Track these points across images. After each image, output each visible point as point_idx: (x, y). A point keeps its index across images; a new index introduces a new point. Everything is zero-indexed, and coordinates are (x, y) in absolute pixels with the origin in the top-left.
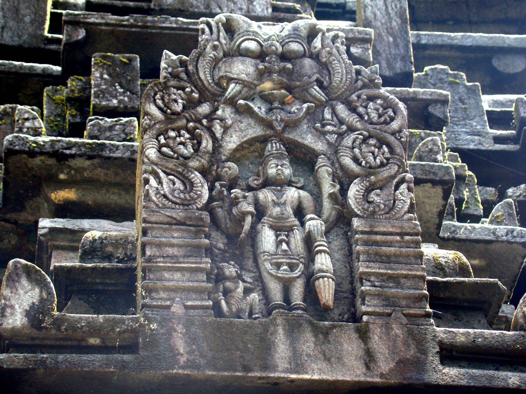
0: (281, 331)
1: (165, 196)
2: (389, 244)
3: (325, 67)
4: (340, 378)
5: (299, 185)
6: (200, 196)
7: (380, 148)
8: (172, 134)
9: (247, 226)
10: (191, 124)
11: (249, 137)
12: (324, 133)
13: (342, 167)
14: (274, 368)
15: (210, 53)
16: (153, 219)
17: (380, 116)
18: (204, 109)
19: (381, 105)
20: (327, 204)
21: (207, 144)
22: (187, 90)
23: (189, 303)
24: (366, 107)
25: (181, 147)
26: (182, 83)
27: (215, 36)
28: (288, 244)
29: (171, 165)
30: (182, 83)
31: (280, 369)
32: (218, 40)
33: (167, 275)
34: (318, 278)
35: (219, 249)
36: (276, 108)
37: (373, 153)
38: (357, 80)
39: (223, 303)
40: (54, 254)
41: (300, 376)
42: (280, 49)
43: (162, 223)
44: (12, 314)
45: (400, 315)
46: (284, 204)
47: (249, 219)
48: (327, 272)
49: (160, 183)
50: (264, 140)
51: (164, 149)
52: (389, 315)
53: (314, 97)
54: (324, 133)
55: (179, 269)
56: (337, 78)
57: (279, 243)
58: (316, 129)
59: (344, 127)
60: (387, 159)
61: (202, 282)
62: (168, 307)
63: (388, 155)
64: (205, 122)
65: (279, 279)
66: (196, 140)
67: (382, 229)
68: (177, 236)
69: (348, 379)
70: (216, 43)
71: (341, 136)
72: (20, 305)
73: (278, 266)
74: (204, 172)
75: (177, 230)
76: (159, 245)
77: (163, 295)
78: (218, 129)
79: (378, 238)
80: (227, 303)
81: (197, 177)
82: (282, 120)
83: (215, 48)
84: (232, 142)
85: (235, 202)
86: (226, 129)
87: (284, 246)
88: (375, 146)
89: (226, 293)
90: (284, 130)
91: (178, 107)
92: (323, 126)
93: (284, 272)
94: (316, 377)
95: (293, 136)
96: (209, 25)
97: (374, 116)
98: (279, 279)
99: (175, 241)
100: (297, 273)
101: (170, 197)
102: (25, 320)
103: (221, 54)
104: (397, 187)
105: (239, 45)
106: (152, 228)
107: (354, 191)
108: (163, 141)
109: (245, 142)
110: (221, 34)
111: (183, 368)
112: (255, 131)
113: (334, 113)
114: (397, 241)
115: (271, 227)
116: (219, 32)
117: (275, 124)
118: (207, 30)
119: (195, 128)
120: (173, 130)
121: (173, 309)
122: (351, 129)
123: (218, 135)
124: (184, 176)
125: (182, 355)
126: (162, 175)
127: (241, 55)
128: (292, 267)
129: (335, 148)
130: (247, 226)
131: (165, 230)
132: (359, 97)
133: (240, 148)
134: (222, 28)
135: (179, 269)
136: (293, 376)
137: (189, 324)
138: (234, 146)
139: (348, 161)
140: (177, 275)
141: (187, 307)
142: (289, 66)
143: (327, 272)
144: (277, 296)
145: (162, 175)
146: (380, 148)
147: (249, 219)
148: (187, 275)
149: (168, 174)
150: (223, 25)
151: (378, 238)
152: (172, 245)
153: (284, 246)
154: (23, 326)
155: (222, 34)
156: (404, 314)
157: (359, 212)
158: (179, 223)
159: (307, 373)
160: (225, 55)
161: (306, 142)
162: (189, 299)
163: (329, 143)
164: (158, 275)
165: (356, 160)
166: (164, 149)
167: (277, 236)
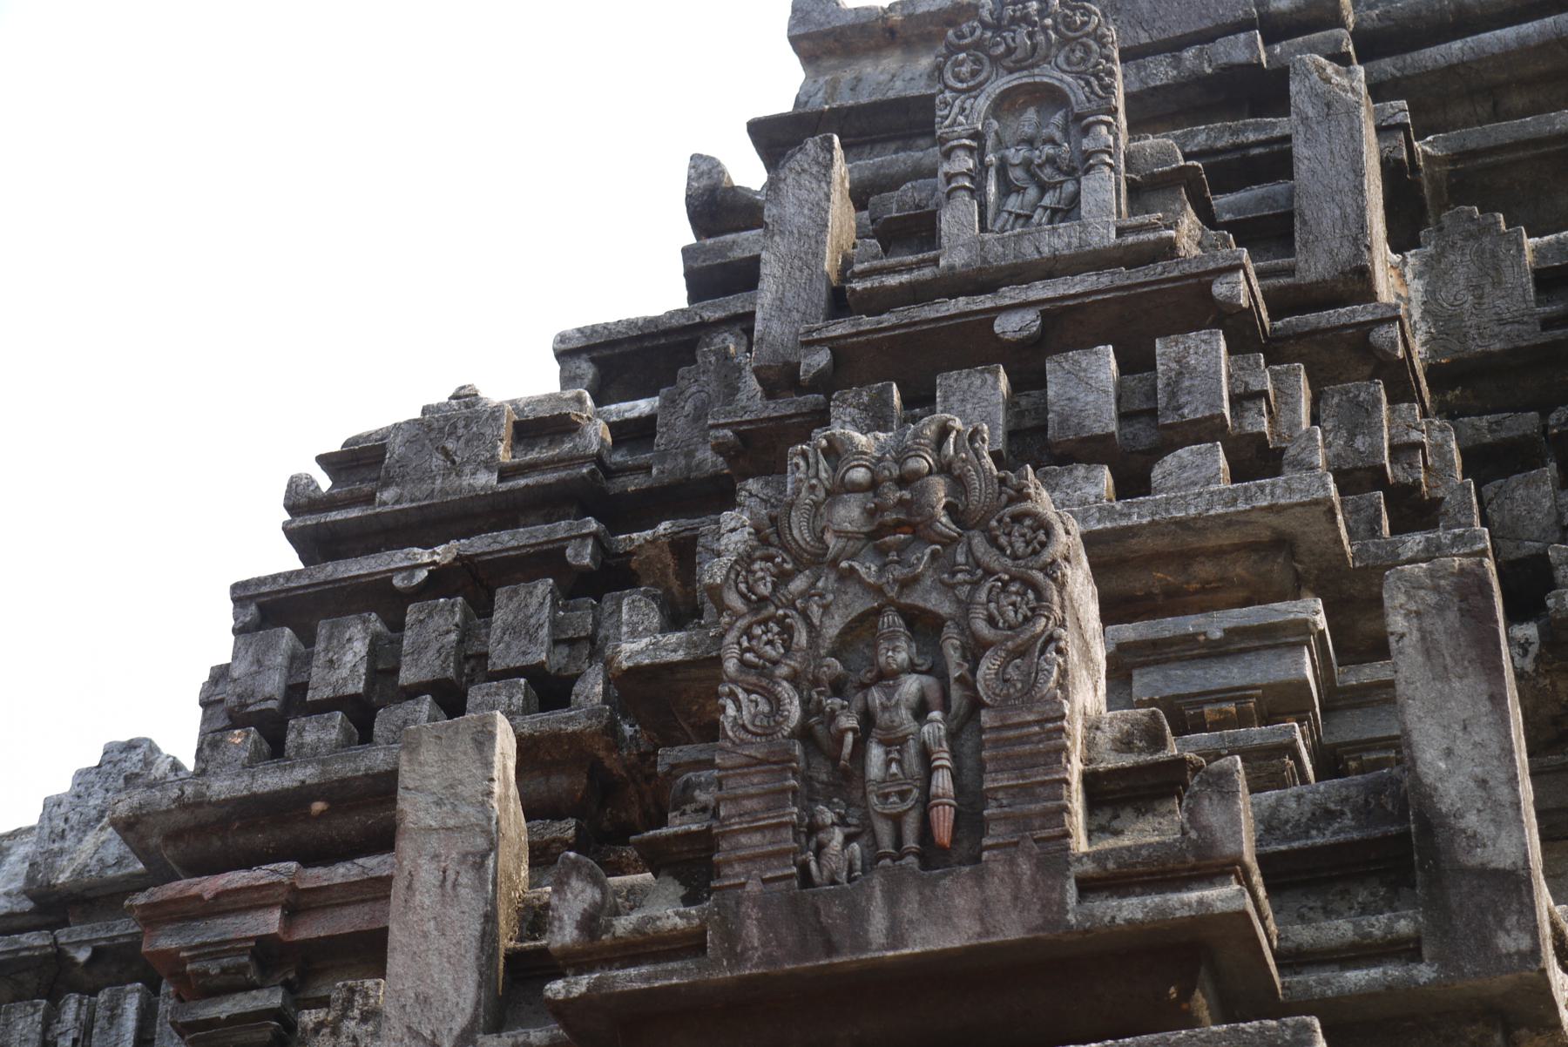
0: (878, 893)
1: (744, 727)
2: (1021, 740)
3: (958, 484)
4: (948, 945)
5: (924, 668)
6: (787, 718)
7: (1023, 595)
8: (758, 631)
9: (847, 749)
10: (781, 612)
11: (854, 614)
12: (953, 587)
13: (974, 635)
14: (866, 946)
15: (806, 498)
16: (729, 763)
17: (1028, 544)
18: (798, 584)
19: (1031, 527)
20: (956, 693)
21: (802, 638)
22: (778, 560)
23: (769, 875)
24: (1009, 534)
25: (768, 648)
26: (772, 551)
27: (812, 472)
28: (900, 763)
29: (753, 679)
30: (772, 551)
31: (874, 947)
32: (817, 476)
33: (744, 840)
34: (937, 805)
35: (822, 783)
36: (892, 562)
37: (1013, 604)
38: (1000, 494)
39: (813, 866)
40: (1136, 673)
41: (898, 953)
42: (896, 472)
43: (740, 767)
44: (561, 928)
45: (1030, 843)
46: (897, 705)
47: (849, 737)
48: (944, 796)
49: (739, 708)
50: (878, 612)
51: (748, 656)
52: (1016, 844)
53: (941, 534)
54: (953, 587)
55: (758, 829)
56: (974, 497)
57: (888, 763)
58: (942, 582)
59: (980, 572)
60: (1033, 610)
61: (787, 839)
62: (743, 885)
63: (1033, 604)
64: (798, 603)
65: (887, 816)
66: (787, 631)
67: (1016, 720)
68: (756, 782)
69: (957, 944)
70: (814, 481)
71: (975, 585)
72: (570, 913)
73: (886, 796)
74: (794, 679)
75: (757, 772)
76: (735, 799)
77: (738, 868)
78: (815, 612)
79: (1011, 733)
80: (818, 863)
81: (785, 689)
82: (895, 580)
83: (812, 488)
84: (833, 628)
85: (833, 716)
86: (826, 609)
87: (894, 768)
88: (1017, 593)
89: (820, 849)
90: (900, 593)
91: (764, 589)
92: (954, 574)
93: (895, 805)
94: (917, 950)
95: (915, 598)
96: (804, 455)
97: (1020, 545)
98: (887, 816)
99: (752, 790)
100: (910, 803)
101: (750, 727)
102: (575, 933)
103: (822, 494)
104: (1042, 652)
105: (843, 478)
106: (727, 777)
107: (988, 667)
108: (745, 644)
109: (852, 621)
110: (821, 466)
111: (756, 966)
112: (862, 604)
113: (970, 551)
114: (1035, 734)
115: (881, 742)
116: (817, 463)
117: (887, 588)
118: (802, 463)
119: (786, 616)
120: (759, 623)
121: (748, 888)
122: (989, 573)
123: (816, 621)
124: (769, 691)
125: (756, 949)
126: (742, 695)
127: (848, 492)
128: (903, 795)
129: (966, 606)
130: (847, 749)
131: (743, 776)
132: (1000, 521)
133: (844, 632)
134: (821, 457)
135: (758, 829)
136: (890, 954)
137: (763, 903)
138: (836, 631)
139: (981, 626)
140: (757, 838)
141: (765, 881)
142: (907, 495)
143: (944, 796)
144: (886, 844)
145: (742, 695)
146: (1023, 595)
147: (849, 737)
148: (769, 835)
149: (748, 692)
150: (823, 450)
151: (1011, 733)
152: (750, 797)
153: (894, 768)
154: (574, 942)
155: (823, 464)
156: (1036, 841)
157: (988, 701)
158: (760, 762)
159: (906, 946)
160: (828, 493)
161: (929, 606)
162: (769, 869)
163: (959, 601)
164: (733, 841)
165: (991, 621)
166: (748, 656)
167: (887, 753)
